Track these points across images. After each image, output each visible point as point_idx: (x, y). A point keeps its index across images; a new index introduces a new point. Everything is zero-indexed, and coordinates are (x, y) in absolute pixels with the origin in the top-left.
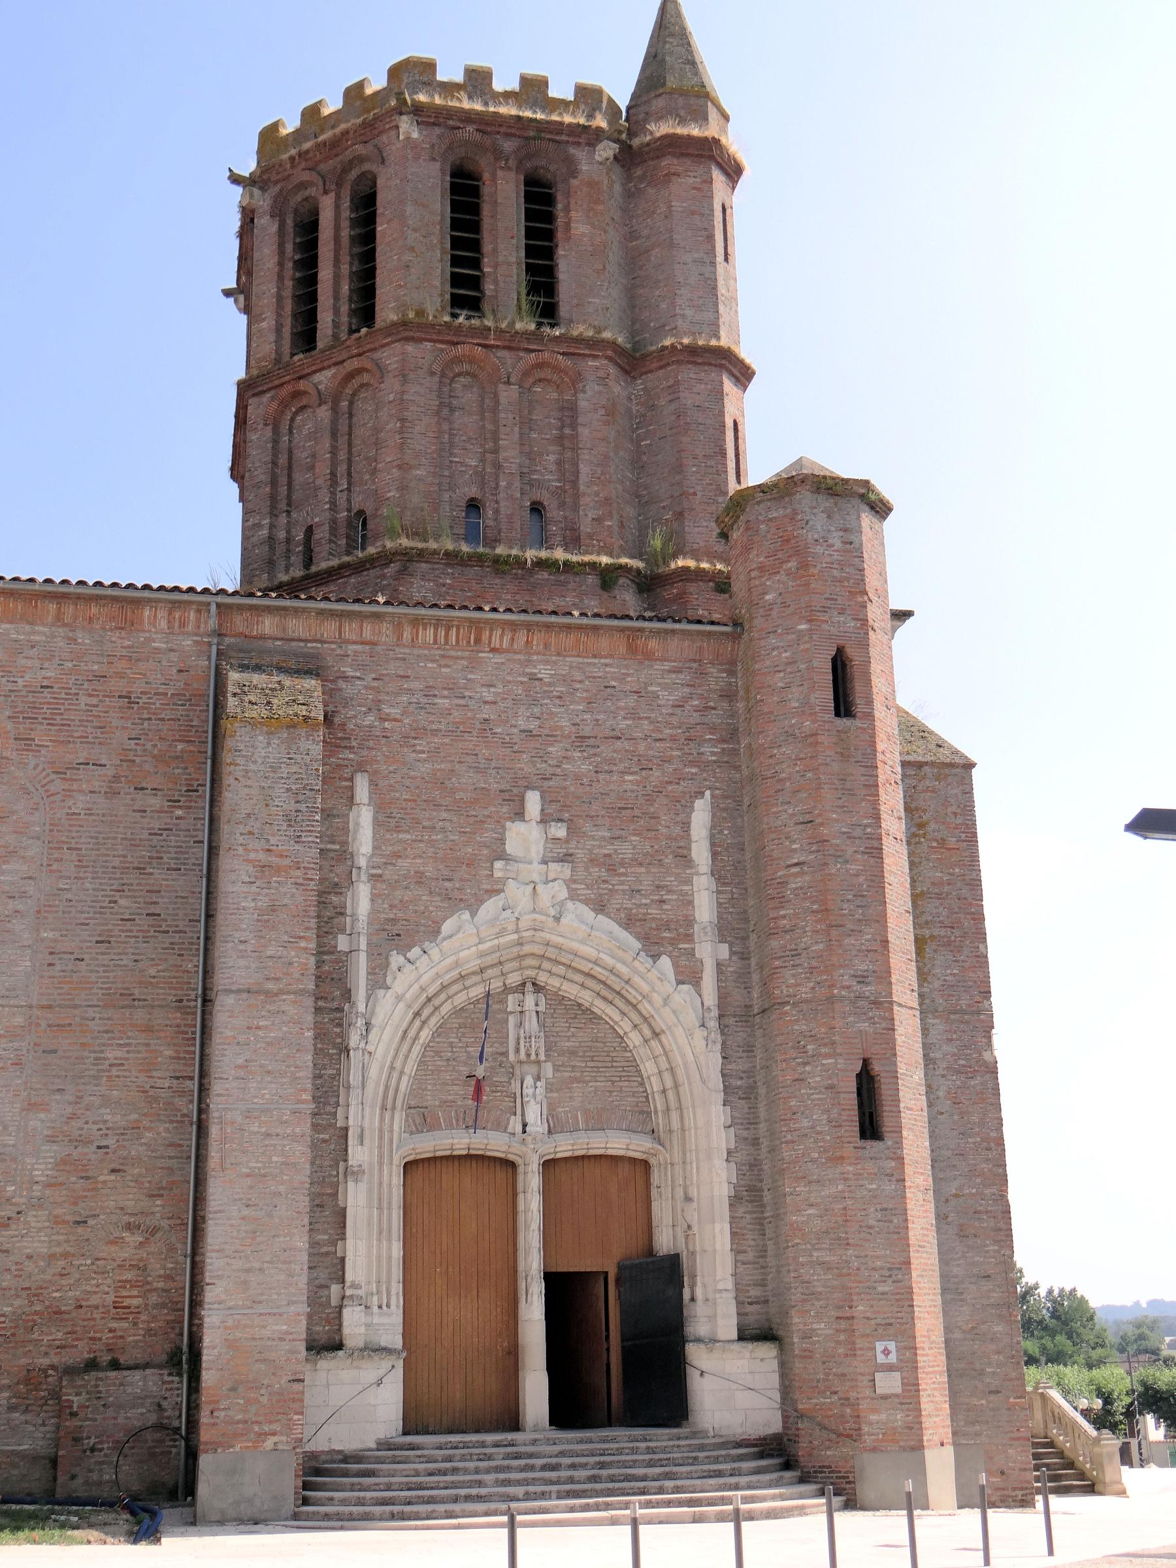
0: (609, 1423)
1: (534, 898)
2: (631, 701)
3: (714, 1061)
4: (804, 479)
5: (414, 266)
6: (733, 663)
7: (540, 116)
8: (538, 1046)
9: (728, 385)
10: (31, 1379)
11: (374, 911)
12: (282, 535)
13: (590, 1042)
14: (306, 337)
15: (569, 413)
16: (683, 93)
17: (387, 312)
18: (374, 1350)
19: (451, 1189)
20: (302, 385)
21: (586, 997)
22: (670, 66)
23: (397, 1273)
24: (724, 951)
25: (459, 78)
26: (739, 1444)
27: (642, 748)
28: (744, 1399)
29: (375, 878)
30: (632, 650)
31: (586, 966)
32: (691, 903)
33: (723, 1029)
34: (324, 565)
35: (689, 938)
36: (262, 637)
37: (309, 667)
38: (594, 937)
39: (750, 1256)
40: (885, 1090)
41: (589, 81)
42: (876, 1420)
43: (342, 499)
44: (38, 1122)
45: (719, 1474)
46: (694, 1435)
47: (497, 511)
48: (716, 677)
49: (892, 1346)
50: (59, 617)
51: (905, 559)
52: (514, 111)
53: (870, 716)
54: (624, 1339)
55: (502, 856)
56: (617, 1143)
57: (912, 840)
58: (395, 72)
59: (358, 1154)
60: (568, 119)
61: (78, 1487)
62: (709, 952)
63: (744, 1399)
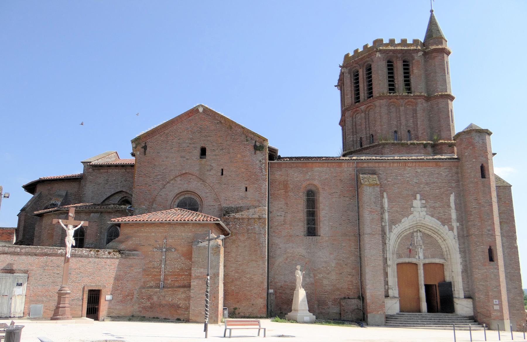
0: (438, 312)
1: (419, 215)
2: (437, 175)
3: (457, 246)
4: (473, 130)
5: (380, 84)
6: (458, 166)
7: (406, 48)
8: (421, 242)
9: (449, 101)
10: (335, 300)
11: (389, 218)
12: (355, 139)
13: (431, 242)
14: (357, 99)
15: (415, 111)
16: (436, 38)
17: (376, 93)
18: (395, 297)
19: (406, 270)
20: (358, 109)
21: (430, 233)
22: (433, 32)
23: (397, 284)
24: (458, 224)
25: (388, 42)
26: (466, 317)
27: (439, 185)
28: (468, 309)
29: (388, 212)
30: (437, 165)
31: (430, 227)
32: (451, 215)
33: (459, 239)
34: (366, 146)
35: (451, 222)
36: (364, 167)
37: (374, 173)
38: (432, 222)
39: (466, 282)
40: (494, 252)
41: (416, 38)
42: (494, 314)
43: (368, 132)
44: (332, 256)
45: (463, 322)
46: (457, 315)
47: (401, 133)
48: (454, 170)
49: (497, 301)
50: (328, 166)
51: (494, 143)
52: (400, 48)
53: (489, 178)
54: (440, 297)
55: (413, 207)
56: (437, 261)
57: (499, 202)
58: (375, 42)
59: (389, 263)
60: (412, 48)
61: (345, 318)
62: (455, 224)
63: (468, 309)
